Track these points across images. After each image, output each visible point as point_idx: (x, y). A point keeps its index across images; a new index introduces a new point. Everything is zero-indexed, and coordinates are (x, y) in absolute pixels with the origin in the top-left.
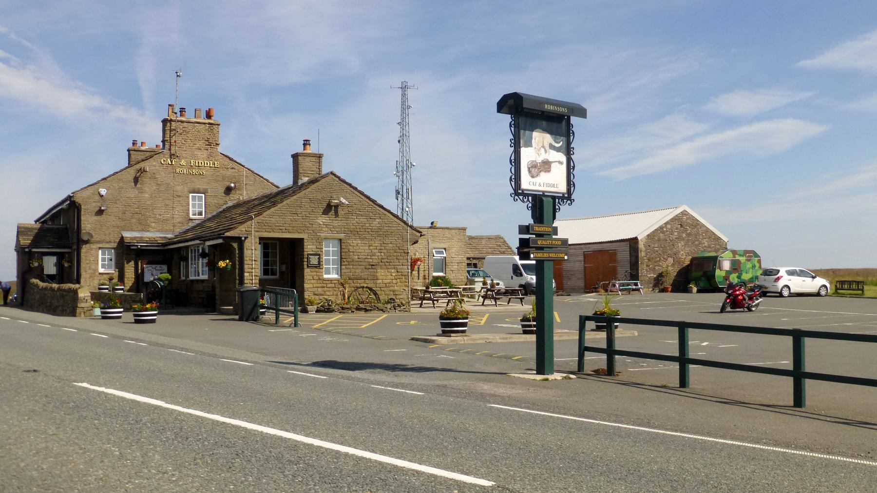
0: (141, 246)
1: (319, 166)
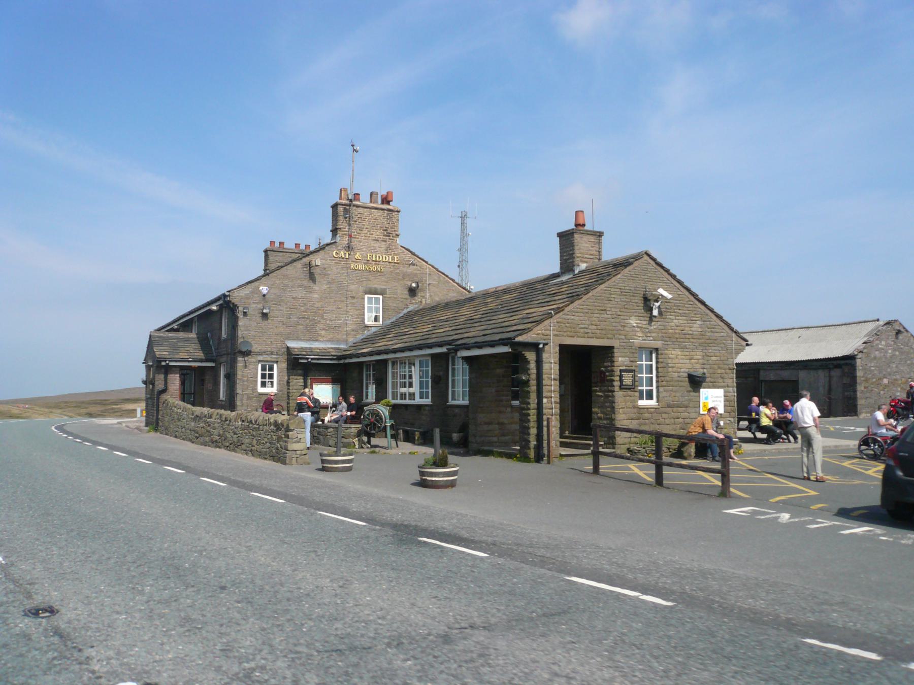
0: (312, 359)
1: (599, 248)
